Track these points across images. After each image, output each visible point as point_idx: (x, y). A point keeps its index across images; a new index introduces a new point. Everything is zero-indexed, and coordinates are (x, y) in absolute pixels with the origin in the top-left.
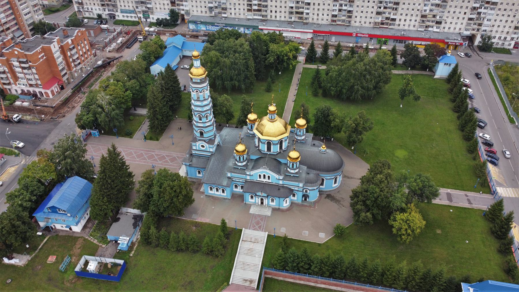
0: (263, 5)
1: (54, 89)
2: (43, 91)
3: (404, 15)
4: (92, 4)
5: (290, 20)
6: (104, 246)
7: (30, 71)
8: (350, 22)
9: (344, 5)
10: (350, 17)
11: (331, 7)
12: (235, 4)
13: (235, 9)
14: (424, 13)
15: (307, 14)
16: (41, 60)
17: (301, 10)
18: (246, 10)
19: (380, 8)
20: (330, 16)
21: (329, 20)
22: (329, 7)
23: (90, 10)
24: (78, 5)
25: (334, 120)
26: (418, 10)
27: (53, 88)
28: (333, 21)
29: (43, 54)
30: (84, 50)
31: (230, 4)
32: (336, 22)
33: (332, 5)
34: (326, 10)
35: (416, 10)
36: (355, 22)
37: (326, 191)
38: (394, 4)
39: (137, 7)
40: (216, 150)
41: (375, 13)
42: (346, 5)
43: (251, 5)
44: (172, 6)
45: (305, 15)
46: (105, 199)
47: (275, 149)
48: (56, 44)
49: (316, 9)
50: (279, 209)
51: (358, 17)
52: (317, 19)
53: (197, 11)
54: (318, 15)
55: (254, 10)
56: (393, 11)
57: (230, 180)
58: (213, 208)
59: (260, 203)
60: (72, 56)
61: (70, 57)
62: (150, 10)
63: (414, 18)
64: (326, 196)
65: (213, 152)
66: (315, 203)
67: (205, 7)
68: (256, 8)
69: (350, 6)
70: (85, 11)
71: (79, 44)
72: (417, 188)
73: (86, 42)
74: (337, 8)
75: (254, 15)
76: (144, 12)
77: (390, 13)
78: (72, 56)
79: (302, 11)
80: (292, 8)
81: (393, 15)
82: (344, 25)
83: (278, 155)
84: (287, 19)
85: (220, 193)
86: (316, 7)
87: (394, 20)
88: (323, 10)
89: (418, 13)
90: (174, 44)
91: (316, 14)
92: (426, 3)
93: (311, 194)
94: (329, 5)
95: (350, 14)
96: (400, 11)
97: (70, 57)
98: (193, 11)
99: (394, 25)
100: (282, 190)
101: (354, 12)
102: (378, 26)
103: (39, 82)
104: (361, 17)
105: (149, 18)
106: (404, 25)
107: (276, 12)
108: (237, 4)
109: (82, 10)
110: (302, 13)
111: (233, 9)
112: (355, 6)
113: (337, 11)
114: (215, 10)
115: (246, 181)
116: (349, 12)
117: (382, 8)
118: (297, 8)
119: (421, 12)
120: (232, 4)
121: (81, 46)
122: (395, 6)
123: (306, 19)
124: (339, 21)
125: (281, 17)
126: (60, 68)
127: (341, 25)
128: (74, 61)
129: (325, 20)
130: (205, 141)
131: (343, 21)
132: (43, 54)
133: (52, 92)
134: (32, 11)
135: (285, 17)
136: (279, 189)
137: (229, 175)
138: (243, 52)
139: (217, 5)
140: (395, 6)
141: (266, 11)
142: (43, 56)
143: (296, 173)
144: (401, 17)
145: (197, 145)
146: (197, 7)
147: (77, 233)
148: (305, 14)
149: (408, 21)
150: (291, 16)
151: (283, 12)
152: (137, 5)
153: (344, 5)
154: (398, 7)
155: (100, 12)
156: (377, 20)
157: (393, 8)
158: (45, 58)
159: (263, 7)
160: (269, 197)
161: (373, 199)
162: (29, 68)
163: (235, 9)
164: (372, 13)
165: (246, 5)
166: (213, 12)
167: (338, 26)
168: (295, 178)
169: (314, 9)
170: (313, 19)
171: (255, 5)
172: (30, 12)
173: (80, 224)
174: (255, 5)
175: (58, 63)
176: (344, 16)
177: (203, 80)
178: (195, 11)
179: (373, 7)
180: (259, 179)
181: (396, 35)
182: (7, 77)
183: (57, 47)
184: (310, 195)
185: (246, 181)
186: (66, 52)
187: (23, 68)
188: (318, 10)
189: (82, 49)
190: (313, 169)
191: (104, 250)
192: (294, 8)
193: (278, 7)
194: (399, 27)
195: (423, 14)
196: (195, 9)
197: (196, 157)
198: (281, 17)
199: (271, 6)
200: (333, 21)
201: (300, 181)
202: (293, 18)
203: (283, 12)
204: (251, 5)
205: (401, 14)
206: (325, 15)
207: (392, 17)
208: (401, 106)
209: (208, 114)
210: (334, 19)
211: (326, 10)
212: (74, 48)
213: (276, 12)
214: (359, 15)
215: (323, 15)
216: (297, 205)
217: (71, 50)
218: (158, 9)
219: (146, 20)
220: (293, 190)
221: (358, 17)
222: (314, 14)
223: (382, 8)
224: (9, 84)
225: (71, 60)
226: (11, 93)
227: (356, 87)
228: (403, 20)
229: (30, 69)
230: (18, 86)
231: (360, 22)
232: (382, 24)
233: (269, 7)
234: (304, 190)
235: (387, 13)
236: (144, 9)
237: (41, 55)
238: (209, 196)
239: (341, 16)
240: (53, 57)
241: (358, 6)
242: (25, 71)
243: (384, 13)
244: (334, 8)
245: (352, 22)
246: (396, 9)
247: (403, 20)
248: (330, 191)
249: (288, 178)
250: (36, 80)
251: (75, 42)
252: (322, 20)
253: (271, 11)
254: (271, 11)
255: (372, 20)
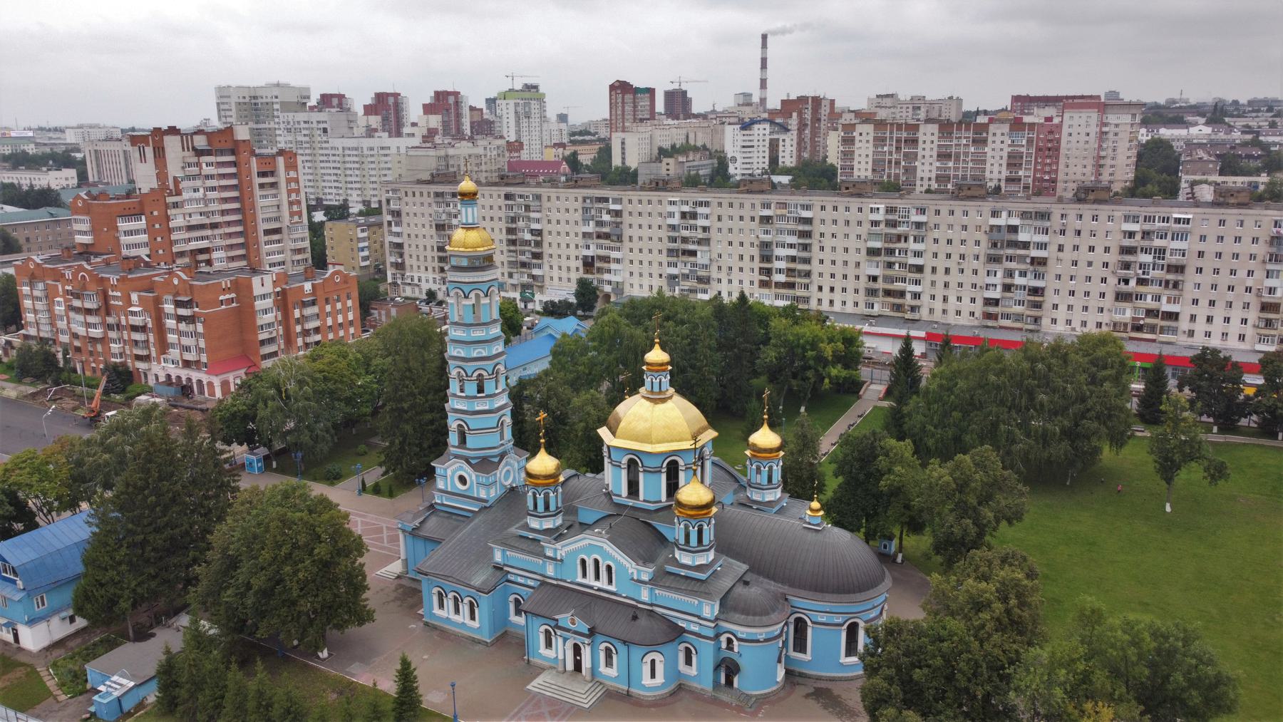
0: (800, 271)
1: (231, 380)
2: (205, 378)
3: (1204, 303)
4: (423, 268)
5: (868, 311)
6: (63, 698)
7: (191, 327)
8: (1036, 320)
9: (1017, 273)
10: (1038, 306)
11: (983, 279)
12: (730, 268)
13: (730, 281)
14: (1267, 298)
15: (916, 296)
16: (223, 307)
17: (898, 286)
18: (756, 284)
19: (1126, 282)
20: (979, 302)
21: (976, 315)
22: (974, 279)
23: (416, 281)
24: (394, 271)
25: (890, 471)
26: (1249, 290)
27: (231, 377)
28: (988, 316)
29: (233, 295)
30: (340, 319)
31: (720, 268)
32: (996, 319)
33: (982, 272)
34: (967, 286)
35: (1240, 289)
36: (1054, 321)
37: (819, 678)
38: (1168, 271)
39: (511, 275)
40: (500, 500)
41: (1110, 296)
42: (1023, 274)
43: (768, 272)
44: (587, 272)
45: (908, 300)
46: (123, 551)
47: (653, 489)
48: (268, 280)
49: (940, 285)
50: (627, 696)
51: (1063, 308)
52: (944, 311)
53: (641, 286)
54: (945, 299)
55: (778, 285)
56: (1167, 292)
57: (499, 573)
58: (425, 657)
59: (570, 666)
60: (304, 319)
61: (298, 321)
62: (537, 281)
63: (1236, 314)
64: (812, 690)
65: (486, 501)
66: (764, 700)
67: (661, 275)
68: (781, 278)
69: (1037, 276)
70: (406, 284)
71: (331, 301)
72: (1132, 652)
73: (349, 303)
74: (999, 279)
75: (777, 297)
76: (525, 287)
77: (1157, 298)
78: (304, 319)
79: (902, 288)
80: (875, 279)
81: (1169, 301)
82: (1021, 329)
83: (660, 514)
84: (862, 310)
85: (464, 617)
86: (940, 277)
87: (1173, 316)
88: (960, 285)
89: (1249, 297)
90: (550, 331)
91: (939, 298)
92: (1270, 267)
93: (746, 656)
94: (975, 272)
95: (1037, 299)
96: (1189, 291)
97: (298, 321)
98: (632, 285)
99: (1174, 331)
100: (643, 621)
101: (1049, 293)
102: (1124, 335)
103: (204, 359)
104: (1070, 307)
105: (532, 301)
106: (1208, 334)
107: (832, 289)
108: (736, 270)
109: (399, 282)
110: (902, 294)
111: (725, 281)
112: (1050, 276)
113: (999, 288)
114: (682, 283)
115: (543, 583)
116: (1036, 291)
117: (1133, 283)
118: (890, 280)
119: (1259, 295)
120: (724, 269)
121: (334, 307)
122: (1171, 277)
123: (913, 309)
124: (1008, 317)
125: (844, 303)
126: (263, 336)
127: (1012, 329)
128: (306, 333)
129: (965, 313)
130: (467, 460)
131: (1019, 318)
132: (233, 295)
133: (225, 384)
134: (289, 259)
135: (856, 304)
136: (635, 618)
137: (498, 557)
138: (689, 322)
139: (686, 271)
140: (1171, 277)
141: (807, 287)
142: (232, 300)
143: (700, 568)
144: (1194, 310)
145: (449, 472)
146: (641, 275)
147: (29, 653)
148: (908, 296)
149: (1218, 320)
150: (871, 299)
151: (850, 290)
152: (512, 270)
153: (1017, 273)
154: (1180, 278)
155: (434, 287)
156: (1118, 317)
157: (1167, 282)
158: (234, 305)
159: (800, 276)
160: (599, 638)
161: (939, 662)
162: (191, 320)
163: (730, 281)
164: (1103, 295)
165: (757, 271)
166: (677, 288)
167: (1002, 330)
168: (693, 584)
169: (933, 283)
170: (931, 311)
171: (780, 271)
172: (284, 263)
173: (42, 626)
174: (780, 271)
175: (259, 322)
176: (1020, 303)
177: (477, 264)
178: (636, 286)
179: (1104, 280)
180: (580, 580)
181: (1179, 355)
182: (147, 341)
183: (269, 288)
184: (741, 662)
185: (543, 583)
186: (290, 306)
187: (180, 319)
188: (946, 285)
189: (334, 314)
190: (768, 577)
191: (56, 707)
192: (880, 280)
193: (839, 276)
194: (1190, 339)
195: (1264, 300)
196: (636, 280)
197: (442, 514)
198: (844, 303)
199: (821, 275)
200: (988, 316)
201: (707, 595)
202: (876, 306)
203: (850, 290)
204: (768, 272)
205: (1195, 302)
206: (966, 300)
207: (1166, 307)
208: (1168, 509)
209: (485, 373)
210: (992, 310)
211: (967, 286)
212: (313, 303)
213: (832, 289)
214: (1063, 300)
215: (959, 299)
216: (697, 696)
217: (304, 305)
218: (556, 279)
219: (526, 306)
220: (683, 630)
221: (1063, 308)
222: (933, 297)
223: (1133, 283)
224: (146, 358)
225: (298, 329)
226: (146, 382)
227: (1002, 427)
228: (1201, 319)
229: (194, 322)
230: (163, 364)
231: (1069, 322)
232: (1138, 328)
233: (815, 276)
234: (723, 638)
235: (1149, 297)
236: (525, 279)
237: (228, 296)
238: (435, 628)
239: (1012, 303)
240: (252, 306)
241: (1059, 277)
242: (183, 326)
243: (1140, 297)
244: (991, 280)
245: (1046, 322)
246: (1176, 285)
247: (1201, 319)
248: (832, 680)
249: (669, 581)
250: (200, 350)
251: (319, 293)
252: (958, 313)
253: (820, 288)
254: (820, 288)
255: (1105, 318)
